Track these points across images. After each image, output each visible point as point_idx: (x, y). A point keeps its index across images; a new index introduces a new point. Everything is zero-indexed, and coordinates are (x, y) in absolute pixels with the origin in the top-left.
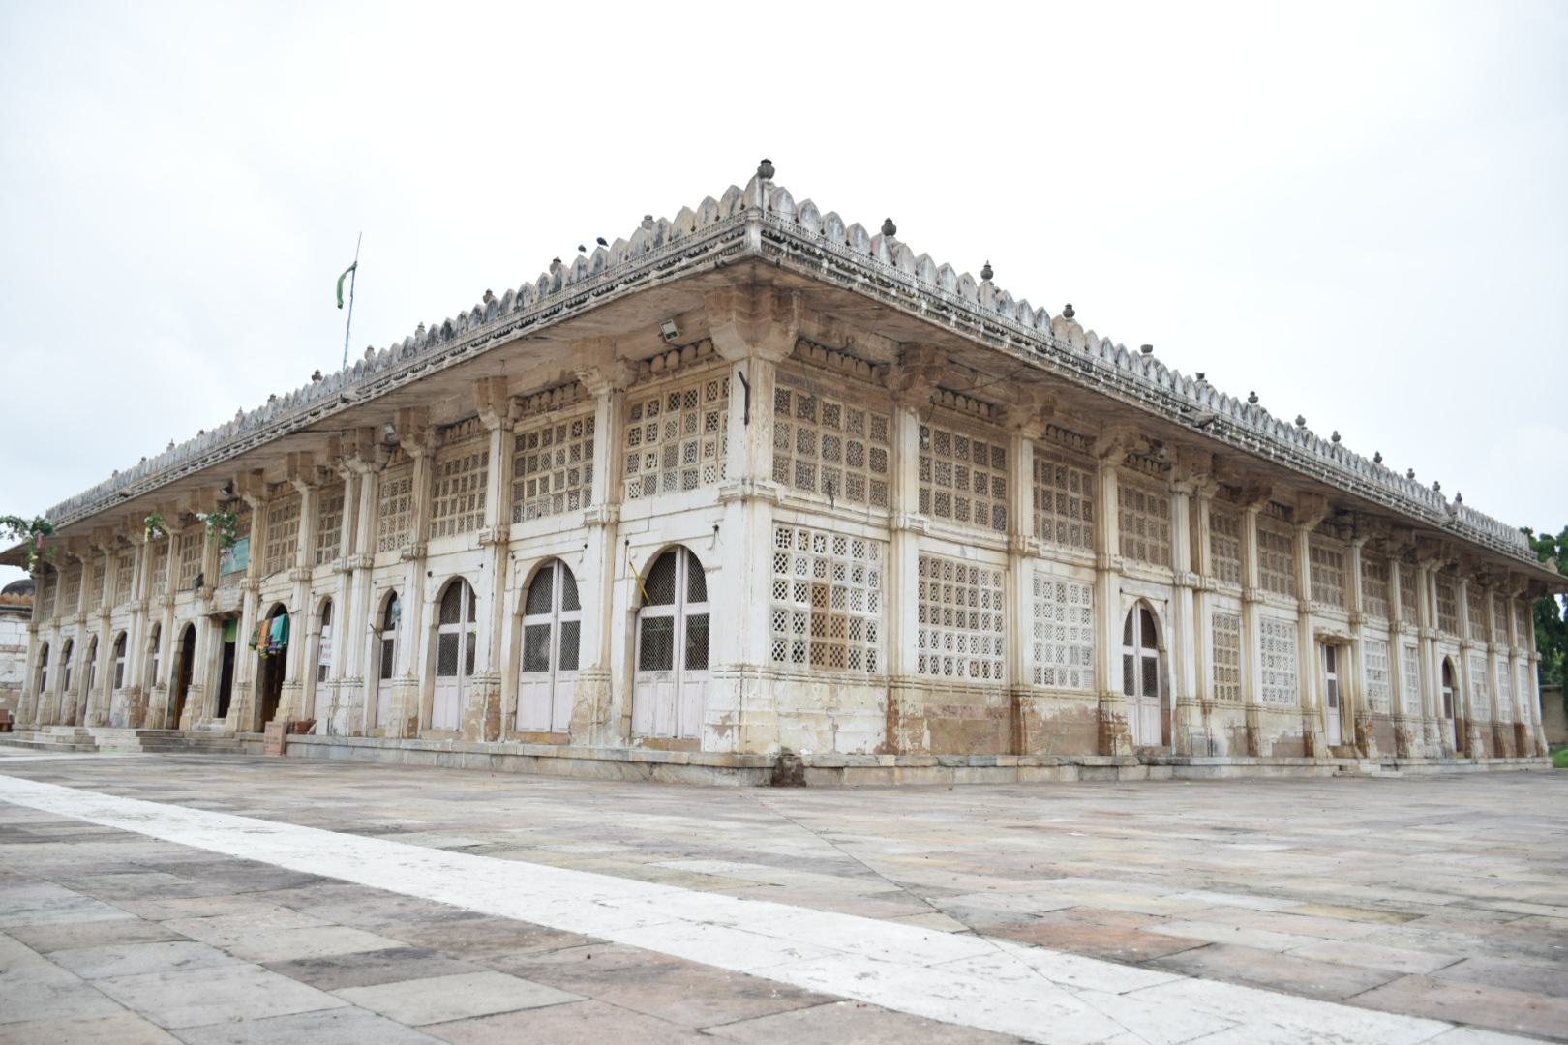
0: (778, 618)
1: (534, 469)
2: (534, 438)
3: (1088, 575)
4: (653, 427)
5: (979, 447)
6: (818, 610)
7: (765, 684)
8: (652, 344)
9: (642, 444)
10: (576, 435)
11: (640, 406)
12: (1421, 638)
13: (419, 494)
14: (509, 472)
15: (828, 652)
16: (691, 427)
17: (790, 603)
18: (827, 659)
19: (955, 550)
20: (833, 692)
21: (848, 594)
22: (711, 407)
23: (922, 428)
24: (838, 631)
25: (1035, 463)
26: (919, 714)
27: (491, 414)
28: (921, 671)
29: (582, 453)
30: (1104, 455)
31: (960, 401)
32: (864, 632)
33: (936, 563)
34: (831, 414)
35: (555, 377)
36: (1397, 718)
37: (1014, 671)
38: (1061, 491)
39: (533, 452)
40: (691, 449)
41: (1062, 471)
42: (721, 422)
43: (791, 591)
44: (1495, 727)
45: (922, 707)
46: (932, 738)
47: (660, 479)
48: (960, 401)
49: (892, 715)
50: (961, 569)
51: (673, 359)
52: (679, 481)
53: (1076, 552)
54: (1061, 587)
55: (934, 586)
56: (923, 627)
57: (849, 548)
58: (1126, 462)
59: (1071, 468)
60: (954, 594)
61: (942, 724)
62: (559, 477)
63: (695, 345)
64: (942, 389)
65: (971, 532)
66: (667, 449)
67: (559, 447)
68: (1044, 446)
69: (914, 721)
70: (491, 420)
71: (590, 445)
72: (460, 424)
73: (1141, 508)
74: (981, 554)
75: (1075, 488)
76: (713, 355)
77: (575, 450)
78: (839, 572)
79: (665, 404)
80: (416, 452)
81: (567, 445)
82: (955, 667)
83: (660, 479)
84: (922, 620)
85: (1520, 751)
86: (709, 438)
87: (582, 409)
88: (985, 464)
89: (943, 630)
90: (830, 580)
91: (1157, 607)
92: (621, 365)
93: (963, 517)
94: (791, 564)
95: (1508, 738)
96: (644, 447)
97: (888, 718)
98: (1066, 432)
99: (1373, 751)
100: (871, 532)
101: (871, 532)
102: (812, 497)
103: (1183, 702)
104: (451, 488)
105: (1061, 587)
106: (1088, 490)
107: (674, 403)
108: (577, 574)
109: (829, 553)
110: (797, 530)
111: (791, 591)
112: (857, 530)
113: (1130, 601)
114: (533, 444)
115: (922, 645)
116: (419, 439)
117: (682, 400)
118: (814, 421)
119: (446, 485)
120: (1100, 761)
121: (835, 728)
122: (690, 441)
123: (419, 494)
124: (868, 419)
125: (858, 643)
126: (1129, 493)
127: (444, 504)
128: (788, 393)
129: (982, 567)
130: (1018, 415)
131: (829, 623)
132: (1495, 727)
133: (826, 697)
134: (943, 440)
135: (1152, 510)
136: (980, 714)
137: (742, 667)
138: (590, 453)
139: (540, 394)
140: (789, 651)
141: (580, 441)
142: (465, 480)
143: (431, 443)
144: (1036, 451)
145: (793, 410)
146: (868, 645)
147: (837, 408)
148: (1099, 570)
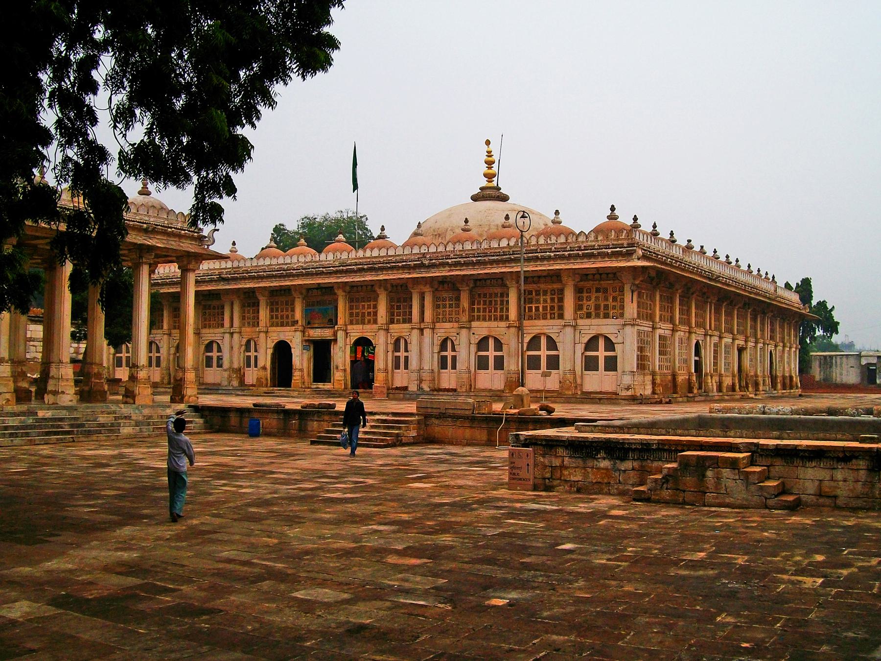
3: (687, 334)
12: (764, 344)
13: (465, 303)
36: (756, 376)
37: (674, 368)
44: (784, 377)
47: (593, 314)
83: (593, 314)
85: (791, 388)
95: (788, 381)
99: (750, 389)
103: (706, 375)
107: (598, 290)
123: (465, 303)
130: (677, 286)
132: (784, 377)
143: (471, 285)
148: (690, 333)
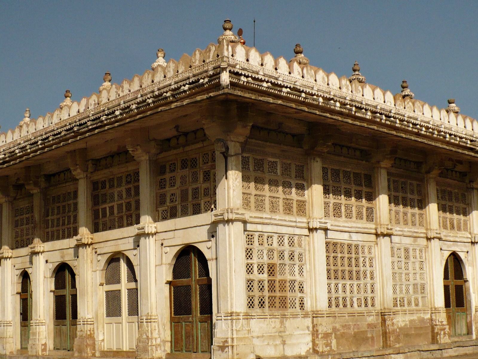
0: (250, 284)
1: (104, 202)
2: (104, 183)
4: (173, 179)
5: (356, 175)
6: (271, 278)
7: (245, 322)
8: (170, 132)
9: (167, 189)
10: (128, 183)
11: (164, 167)
14: (90, 203)
15: (277, 301)
16: (195, 180)
17: (256, 276)
18: (277, 305)
19: (346, 236)
20: (282, 323)
21: (287, 267)
22: (205, 168)
23: (323, 168)
24: (283, 289)
25: (389, 180)
26: (330, 331)
27: (79, 171)
28: (330, 306)
29: (133, 193)
30: (428, 172)
31: (345, 150)
32: (297, 288)
33: (335, 244)
34: (273, 166)
35: (115, 149)
38: (404, 195)
39: (103, 191)
40: (196, 192)
41: (405, 183)
42: (212, 176)
43: (255, 269)
45: (331, 327)
46: (338, 343)
47: (179, 209)
48: (345, 150)
49: (315, 333)
50: (349, 246)
51: (182, 140)
52: (190, 209)
53: (414, 229)
54: (407, 250)
55: (335, 258)
56: (330, 281)
57: (286, 241)
58: (441, 175)
59: (409, 181)
60: (346, 261)
61: (343, 335)
62: (120, 206)
63: (195, 132)
64: (335, 145)
65: (354, 225)
66: (182, 191)
67: (119, 189)
68: (393, 170)
69: (327, 336)
70: (78, 173)
71: (137, 188)
72: (59, 174)
73: (450, 200)
74: (360, 237)
75: (412, 192)
76: (205, 137)
77: (128, 191)
78: (281, 255)
79: (179, 164)
80: (35, 191)
81: (123, 189)
82: (348, 303)
83: (179, 209)
84: (329, 278)
86: (205, 186)
87: (131, 167)
88: (360, 185)
89: (341, 283)
90: (276, 260)
91: (462, 255)
92: (153, 143)
93: (349, 216)
94: (255, 255)
96: (169, 190)
97: (313, 335)
98: (406, 161)
100: (298, 231)
101: (298, 231)
102: (264, 216)
104: (56, 211)
105: (407, 250)
106: (420, 193)
107: (184, 165)
108: (135, 262)
109: (275, 244)
110: (257, 234)
111: (255, 269)
112: (290, 231)
113: (447, 254)
114: (104, 187)
115: (329, 292)
116: (36, 184)
117: (189, 163)
118: (263, 171)
119: (53, 209)
120: (433, 347)
121: (284, 343)
122: (195, 186)
124: (293, 167)
125: (293, 294)
126: (443, 192)
127: (53, 221)
128: (248, 158)
129: (360, 244)
131: (277, 284)
133: (278, 325)
134: (336, 173)
135: (457, 200)
136: (364, 328)
137: (231, 314)
138: (137, 193)
139: (105, 158)
140: (256, 302)
141: (131, 186)
142: (64, 207)
144: (389, 174)
145: (251, 168)
146: (300, 295)
147: (276, 162)
